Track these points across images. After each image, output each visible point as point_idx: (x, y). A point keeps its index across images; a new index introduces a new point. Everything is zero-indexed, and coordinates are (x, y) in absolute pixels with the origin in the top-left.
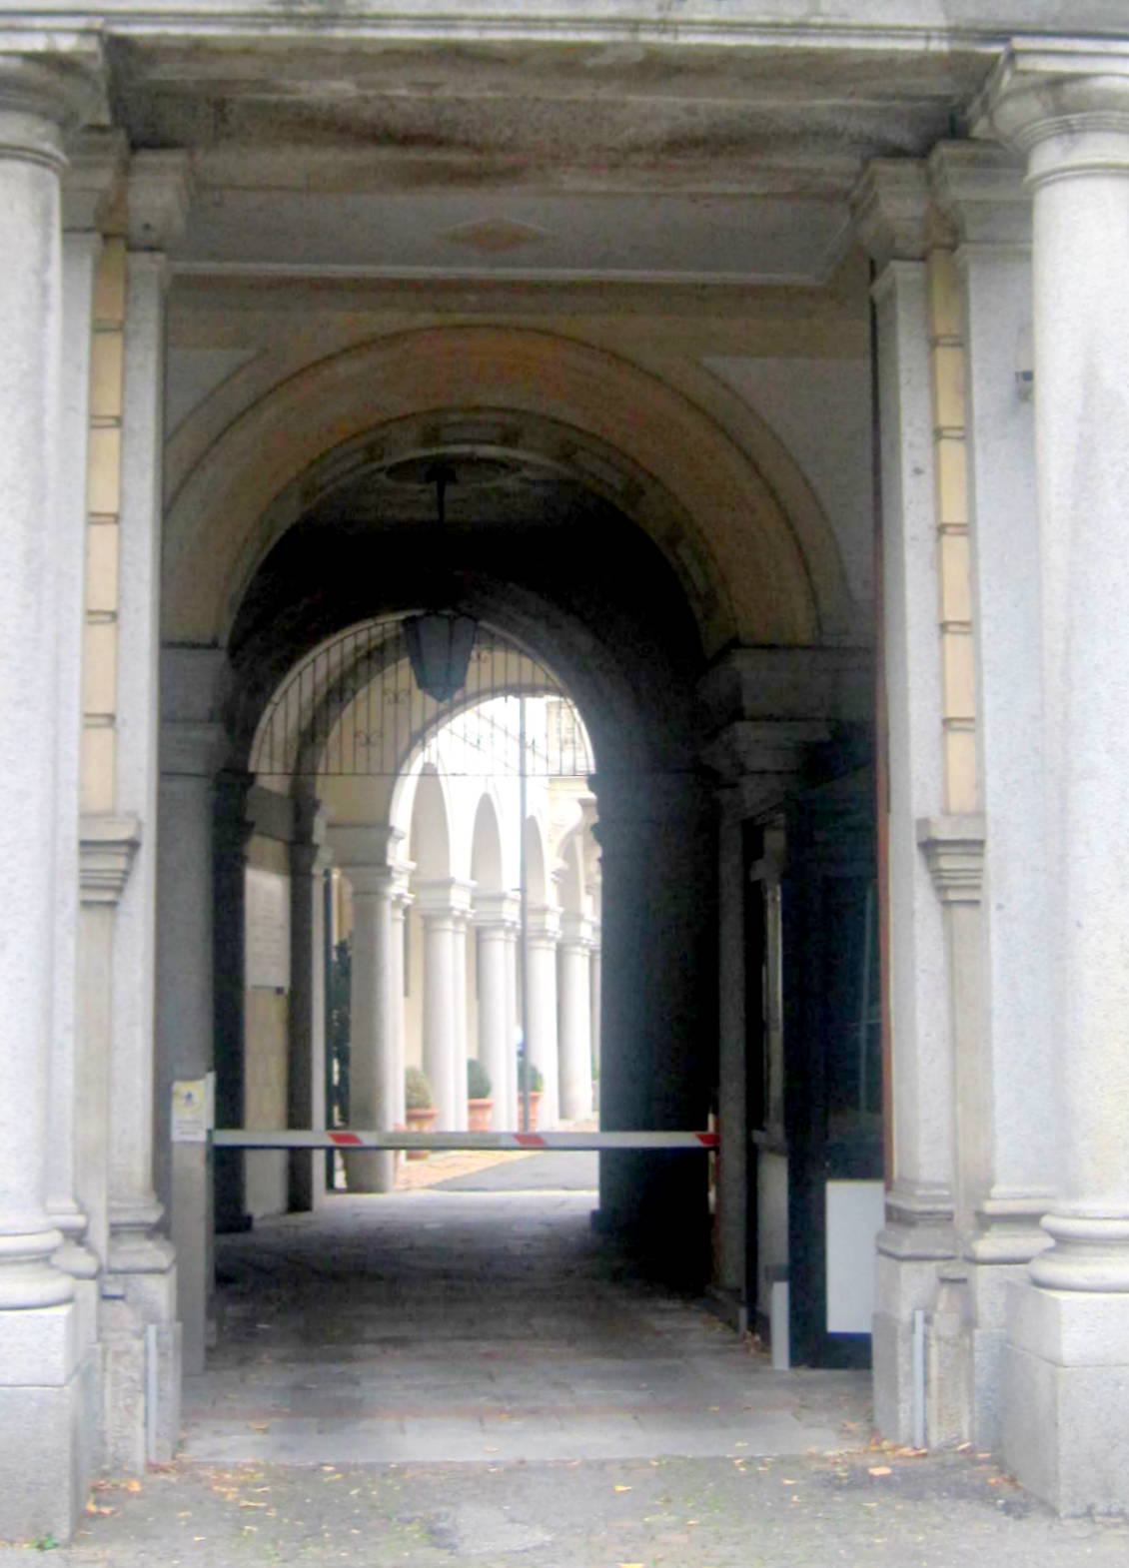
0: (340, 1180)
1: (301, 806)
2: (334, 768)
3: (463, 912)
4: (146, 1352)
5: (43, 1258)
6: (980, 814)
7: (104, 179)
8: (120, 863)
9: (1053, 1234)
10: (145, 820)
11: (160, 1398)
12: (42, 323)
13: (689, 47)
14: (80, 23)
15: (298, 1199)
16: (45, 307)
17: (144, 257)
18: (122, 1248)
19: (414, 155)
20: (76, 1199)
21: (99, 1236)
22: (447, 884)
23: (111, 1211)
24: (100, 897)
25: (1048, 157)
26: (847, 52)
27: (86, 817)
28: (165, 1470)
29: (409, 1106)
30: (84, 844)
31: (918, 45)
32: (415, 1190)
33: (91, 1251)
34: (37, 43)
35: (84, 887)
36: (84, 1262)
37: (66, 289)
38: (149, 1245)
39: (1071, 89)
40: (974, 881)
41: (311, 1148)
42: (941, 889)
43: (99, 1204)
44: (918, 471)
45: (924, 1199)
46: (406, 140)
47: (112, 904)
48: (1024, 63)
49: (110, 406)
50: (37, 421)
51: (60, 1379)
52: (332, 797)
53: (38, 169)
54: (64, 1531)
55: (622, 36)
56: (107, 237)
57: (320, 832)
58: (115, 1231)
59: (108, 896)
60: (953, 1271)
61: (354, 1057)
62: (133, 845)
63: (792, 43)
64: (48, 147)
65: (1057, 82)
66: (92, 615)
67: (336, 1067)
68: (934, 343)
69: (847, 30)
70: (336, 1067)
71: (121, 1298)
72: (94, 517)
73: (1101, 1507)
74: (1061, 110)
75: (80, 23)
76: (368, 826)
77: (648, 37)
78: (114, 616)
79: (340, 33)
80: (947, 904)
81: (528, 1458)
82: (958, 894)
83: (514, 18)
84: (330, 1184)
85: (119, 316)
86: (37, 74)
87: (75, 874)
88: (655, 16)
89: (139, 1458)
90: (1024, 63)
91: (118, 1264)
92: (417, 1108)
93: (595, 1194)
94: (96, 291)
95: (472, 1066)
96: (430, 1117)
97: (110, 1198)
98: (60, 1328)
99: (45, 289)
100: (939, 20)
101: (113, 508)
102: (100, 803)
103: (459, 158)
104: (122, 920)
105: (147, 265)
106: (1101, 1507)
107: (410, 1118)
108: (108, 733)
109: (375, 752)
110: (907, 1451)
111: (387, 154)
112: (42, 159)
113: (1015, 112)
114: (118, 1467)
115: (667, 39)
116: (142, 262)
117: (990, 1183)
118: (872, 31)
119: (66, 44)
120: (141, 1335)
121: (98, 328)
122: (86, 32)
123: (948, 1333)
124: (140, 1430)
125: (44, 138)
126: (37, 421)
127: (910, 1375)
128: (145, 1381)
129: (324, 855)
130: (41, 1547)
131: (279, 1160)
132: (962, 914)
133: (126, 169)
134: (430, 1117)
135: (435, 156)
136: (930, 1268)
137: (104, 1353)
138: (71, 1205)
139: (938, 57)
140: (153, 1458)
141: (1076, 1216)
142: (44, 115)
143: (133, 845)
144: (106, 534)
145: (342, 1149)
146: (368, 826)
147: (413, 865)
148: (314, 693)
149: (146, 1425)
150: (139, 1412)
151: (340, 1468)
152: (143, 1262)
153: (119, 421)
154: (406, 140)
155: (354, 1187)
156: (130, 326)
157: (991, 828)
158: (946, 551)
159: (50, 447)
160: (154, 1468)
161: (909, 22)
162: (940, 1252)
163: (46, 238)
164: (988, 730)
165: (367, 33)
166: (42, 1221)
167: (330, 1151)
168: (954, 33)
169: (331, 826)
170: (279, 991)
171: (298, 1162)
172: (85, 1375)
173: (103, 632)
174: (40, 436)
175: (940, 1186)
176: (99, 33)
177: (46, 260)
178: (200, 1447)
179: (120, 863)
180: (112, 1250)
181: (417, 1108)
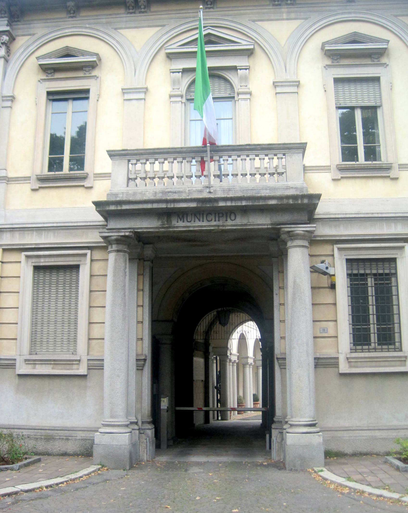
0: (220, 418)
1: (207, 344)
2: (213, 338)
3: (251, 363)
4: (147, 442)
5: (127, 426)
6: (285, 354)
7: (139, 250)
8: (143, 363)
9: (290, 424)
10: (147, 355)
11: (149, 450)
12: (125, 278)
13: (228, 229)
14: (129, 230)
15: (207, 420)
16: (126, 275)
17: (147, 262)
18: (144, 425)
19: (191, 243)
20: (136, 417)
21: (140, 423)
22: (247, 358)
23: (142, 419)
24: (140, 368)
25: (289, 244)
26: (254, 228)
27: (137, 355)
28: (149, 461)
29: (238, 403)
30: (137, 360)
31: (266, 227)
32: (234, 419)
33: (138, 425)
34: (123, 234)
35: (137, 367)
36: (136, 427)
37: (130, 272)
38: (148, 425)
39: (291, 233)
40: (285, 365)
41: (209, 411)
42: (280, 366)
43: (139, 418)
44: (276, 294)
45: (277, 419)
46: (190, 241)
47: (142, 369)
48: (283, 229)
49: (141, 288)
50: (124, 294)
51: (128, 444)
52: (213, 343)
53: (124, 253)
54: (128, 468)
55: (217, 228)
56: (140, 259)
57: (211, 349)
58: (143, 423)
59: (141, 368)
60: (280, 431)
61: (222, 393)
62: (145, 360)
63: (244, 227)
64: (125, 250)
65: (289, 232)
66: (138, 322)
67: (219, 395)
68: (279, 272)
69: (254, 225)
70: (219, 395)
71: (143, 433)
72: (138, 306)
73: (294, 469)
74: (290, 236)
75: (129, 230)
76: (224, 348)
77: (220, 228)
78: (142, 322)
79: (171, 230)
80: (281, 368)
81: (209, 461)
82: (283, 367)
83: (199, 226)
84: (214, 418)
85: (142, 272)
86: (122, 238)
87: (135, 364)
88: (222, 224)
89: (145, 459)
90: (283, 229)
91: (143, 428)
92: (240, 402)
93: (261, 421)
94: (138, 268)
95: (254, 395)
96: (243, 405)
97: (142, 417)
98: (127, 436)
99: (125, 273)
100: (269, 222)
101: (142, 304)
102: (140, 352)
103: (199, 243)
104: (144, 372)
105: (148, 264)
106: (294, 469)
107: (238, 406)
108: (141, 341)
109: (218, 335)
110: (273, 461)
111: (186, 243)
112: (125, 252)
113: (283, 237)
114: (142, 461)
115: (224, 228)
116: (146, 263)
117: (287, 416)
118: (258, 225)
119: (127, 234)
120: (146, 439)
121: (138, 275)
122: (130, 232)
123: (279, 441)
124: (145, 455)
125: (125, 248)
126: (124, 294)
127: (274, 448)
128: (147, 447)
129: (211, 354)
130: (124, 470)
131: (202, 414)
132: (283, 370)
133: (143, 248)
134: (243, 405)
135: (195, 243)
136: (277, 430)
137: (140, 442)
138: (135, 418)
139: (269, 228)
140: (148, 459)
141: (292, 421)
142: (125, 245)
143: (145, 360)
144: (140, 309)
145: (220, 411)
146: (224, 348)
147: (238, 354)
148: (209, 323)
149: (147, 454)
150: (146, 452)
151: (178, 462)
152: (147, 427)
153: (143, 290)
154: (190, 241)
155: (222, 419)
156: (144, 274)
157: (287, 356)
158: (281, 308)
159: (127, 297)
160: (147, 461)
161: (264, 223)
162: (279, 428)
163: (126, 264)
164: (286, 339)
165: (176, 229)
166: (127, 420)
167: (218, 411)
168: (272, 224)
169: (213, 348)
170: (202, 381)
171: (207, 414)
172: (134, 445)
173: (140, 325)
174: (125, 296)
175: (280, 416)
176: (132, 232)
177: (126, 268)
178: (157, 458)
179: (143, 363)
180: (142, 425)
181: (240, 402)
